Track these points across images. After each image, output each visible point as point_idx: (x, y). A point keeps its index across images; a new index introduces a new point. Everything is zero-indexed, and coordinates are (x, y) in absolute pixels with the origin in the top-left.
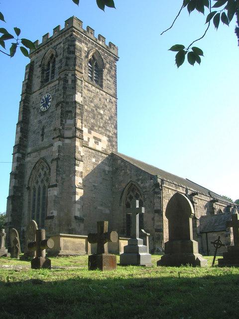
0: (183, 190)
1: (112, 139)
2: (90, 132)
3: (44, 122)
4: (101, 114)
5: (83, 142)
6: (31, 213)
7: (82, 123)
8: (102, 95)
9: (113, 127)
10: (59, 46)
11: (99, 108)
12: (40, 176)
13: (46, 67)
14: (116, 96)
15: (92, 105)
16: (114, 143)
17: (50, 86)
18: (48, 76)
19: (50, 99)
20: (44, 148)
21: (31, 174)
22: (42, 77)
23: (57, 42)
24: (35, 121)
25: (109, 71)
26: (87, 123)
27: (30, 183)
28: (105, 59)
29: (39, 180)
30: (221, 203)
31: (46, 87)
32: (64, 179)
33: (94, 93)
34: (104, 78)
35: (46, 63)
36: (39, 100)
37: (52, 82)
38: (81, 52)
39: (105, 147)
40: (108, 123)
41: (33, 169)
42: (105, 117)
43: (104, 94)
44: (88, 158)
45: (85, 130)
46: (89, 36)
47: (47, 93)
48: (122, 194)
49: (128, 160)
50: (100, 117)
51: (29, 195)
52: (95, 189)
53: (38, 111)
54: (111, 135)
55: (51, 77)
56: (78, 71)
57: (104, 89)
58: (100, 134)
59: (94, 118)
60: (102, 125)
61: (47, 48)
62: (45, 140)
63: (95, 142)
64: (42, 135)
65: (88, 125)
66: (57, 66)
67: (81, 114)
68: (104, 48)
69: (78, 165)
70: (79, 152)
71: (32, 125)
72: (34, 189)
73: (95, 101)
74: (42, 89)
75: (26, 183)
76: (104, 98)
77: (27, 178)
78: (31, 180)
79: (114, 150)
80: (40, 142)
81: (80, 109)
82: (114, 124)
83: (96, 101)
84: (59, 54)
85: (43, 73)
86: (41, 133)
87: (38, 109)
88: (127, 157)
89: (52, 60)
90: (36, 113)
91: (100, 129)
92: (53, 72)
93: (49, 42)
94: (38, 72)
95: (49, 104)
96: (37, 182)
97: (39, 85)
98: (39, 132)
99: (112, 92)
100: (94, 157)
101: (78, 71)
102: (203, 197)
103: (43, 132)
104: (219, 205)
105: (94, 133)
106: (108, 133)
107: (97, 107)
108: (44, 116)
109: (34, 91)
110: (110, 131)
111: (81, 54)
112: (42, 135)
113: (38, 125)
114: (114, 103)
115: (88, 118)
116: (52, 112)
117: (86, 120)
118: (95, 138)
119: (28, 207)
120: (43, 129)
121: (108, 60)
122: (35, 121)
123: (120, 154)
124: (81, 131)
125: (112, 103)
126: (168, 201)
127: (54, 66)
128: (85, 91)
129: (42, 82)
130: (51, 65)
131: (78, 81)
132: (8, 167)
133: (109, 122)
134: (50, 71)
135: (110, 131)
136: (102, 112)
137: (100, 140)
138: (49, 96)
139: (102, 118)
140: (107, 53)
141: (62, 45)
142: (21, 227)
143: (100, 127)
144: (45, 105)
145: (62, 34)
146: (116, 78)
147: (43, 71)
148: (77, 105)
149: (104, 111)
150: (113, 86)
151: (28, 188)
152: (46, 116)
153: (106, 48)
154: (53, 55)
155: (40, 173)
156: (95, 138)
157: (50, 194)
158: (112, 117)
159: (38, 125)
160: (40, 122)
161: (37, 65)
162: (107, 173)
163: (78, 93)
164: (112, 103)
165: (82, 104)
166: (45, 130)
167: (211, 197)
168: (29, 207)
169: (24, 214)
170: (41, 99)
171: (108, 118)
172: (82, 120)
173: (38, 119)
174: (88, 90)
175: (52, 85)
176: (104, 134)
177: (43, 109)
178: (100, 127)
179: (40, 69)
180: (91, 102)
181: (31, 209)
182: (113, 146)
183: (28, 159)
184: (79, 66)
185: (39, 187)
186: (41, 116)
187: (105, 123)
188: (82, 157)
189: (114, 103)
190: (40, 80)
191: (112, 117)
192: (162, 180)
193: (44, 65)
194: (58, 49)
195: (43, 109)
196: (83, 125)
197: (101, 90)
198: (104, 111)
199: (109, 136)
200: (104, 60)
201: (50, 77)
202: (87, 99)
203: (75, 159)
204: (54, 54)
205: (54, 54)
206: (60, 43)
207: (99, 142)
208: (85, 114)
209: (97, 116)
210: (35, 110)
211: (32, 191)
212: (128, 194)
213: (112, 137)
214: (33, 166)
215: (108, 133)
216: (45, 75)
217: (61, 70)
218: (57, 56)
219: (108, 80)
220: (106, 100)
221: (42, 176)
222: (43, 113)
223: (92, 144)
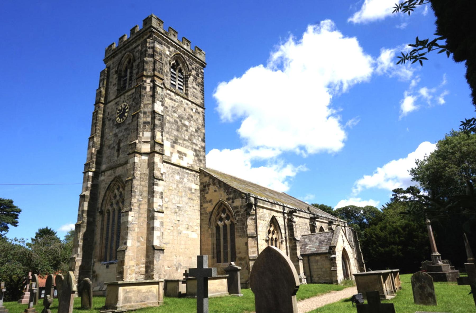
0: (280, 208)
1: (199, 153)
2: (173, 147)
3: (120, 135)
4: (185, 125)
5: (164, 157)
6: (104, 241)
7: (162, 135)
8: (187, 104)
9: (200, 139)
10: (137, 49)
11: (183, 118)
12: (115, 197)
13: (123, 74)
14: (204, 105)
15: (176, 115)
16: (201, 158)
17: (127, 94)
18: (125, 83)
19: (127, 108)
20: (121, 165)
21: (105, 195)
22: (118, 85)
23: (134, 46)
24: (111, 134)
25: (195, 79)
26: (169, 136)
27: (104, 205)
28: (191, 65)
29: (114, 201)
30: (321, 219)
31: (123, 96)
32: (140, 201)
33: (177, 102)
34: (190, 85)
35: (124, 69)
36: (115, 110)
37: (129, 90)
38: (162, 56)
39: (191, 162)
40: (194, 136)
41: (107, 189)
42: (191, 128)
43: (190, 103)
44: (170, 175)
45: (167, 145)
46: (171, 38)
47: (123, 102)
48: (211, 215)
49: (221, 179)
50: (184, 128)
51: (103, 221)
52: (179, 210)
53: (113, 123)
54: (197, 148)
55: (129, 84)
56: (158, 77)
57: (190, 99)
58: (186, 147)
59: (178, 130)
60: (187, 138)
61: (123, 52)
62: (120, 156)
63: (180, 157)
64: (118, 150)
65: (171, 138)
66: (135, 72)
67: (162, 126)
68: (189, 52)
69: (157, 185)
70: (159, 170)
71: (106, 139)
72: (109, 213)
73: (179, 111)
74: (119, 99)
75: (99, 206)
76: (189, 108)
77: (100, 201)
78: (104, 202)
79: (202, 165)
80: (116, 158)
81: (159, 120)
82: (202, 137)
83: (180, 111)
84: (136, 58)
85: (119, 80)
86: (116, 147)
87: (114, 120)
88: (217, 173)
89: (130, 66)
90: (111, 125)
91: (185, 142)
92: (131, 79)
93: (126, 44)
94: (114, 78)
95: (126, 114)
96: (112, 205)
97: (116, 94)
98: (114, 147)
99: (199, 101)
100: (178, 173)
101: (158, 77)
102: (302, 214)
103: (119, 146)
104: (320, 222)
105: (178, 148)
106: (194, 147)
107: (181, 118)
108: (120, 129)
109: (110, 100)
110: (196, 145)
111: (161, 58)
112: (118, 150)
113: (113, 139)
114: (201, 113)
115: (170, 130)
116: (129, 124)
117: (168, 133)
118: (179, 152)
119: (101, 234)
120: (119, 144)
121: (193, 66)
122: (111, 134)
123: (210, 170)
124: (162, 145)
125: (199, 113)
126: (86, 225)
127: (131, 73)
128: (167, 101)
129: (118, 90)
130: (129, 71)
131: (158, 88)
132: (254, 182)
133: (196, 134)
134: (128, 77)
135: (196, 145)
136: (187, 123)
137: (185, 155)
138: (126, 105)
139: (187, 131)
140: (193, 59)
141: (140, 47)
142: (91, 259)
143: (185, 140)
144: (121, 116)
145: (140, 34)
146: (203, 86)
147: (120, 78)
148: (157, 115)
149: (190, 122)
150: (200, 95)
151: (102, 212)
152: (124, 127)
153: (191, 52)
154: (130, 59)
155: (115, 194)
156: (179, 152)
157: (123, 219)
158: (199, 129)
159: (113, 139)
160: (116, 135)
161: (112, 71)
162: (193, 191)
163: (158, 102)
164: (199, 113)
165: (162, 114)
166: (122, 145)
167: (311, 213)
168: (102, 234)
169: (95, 243)
170: (117, 109)
171: (194, 130)
172: (162, 132)
173: (114, 132)
174: (171, 99)
175: (130, 93)
176: (190, 148)
177: (119, 120)
178: (185, 140)
179: (115, 76)
180: (174, 112)
181: (105, 236)
182: (200, 160)
183: (102, 178)
184: (159, 72)
185: (114, 209)
186: (117, 128)
187: (191, 135)
188: (162, 174)
189: (201, 113)
190: (116, 88)
191: (199, 129)
192: (256, 199)
193: (121, 71)
194: (136, 52)
195: (119, 120)
196: (165, 138)
197: (185, 99)
198: (190, 122)
199: (195, 151)
200: (189, 66)
201: (127, 85)
202: (170, 109)
203: (154, 177)
204: (132, 58)
205: (132, 58)
206: (138, 46)
207: (184, 157)
208: (167, 125)
209: (182, 128)
210: (111, 121)
211: (106, 214)
212: (217, 215)
213: (200, 151)
214: (107, 186)
215: (194, 147)
216: (122, 83)
217: (137, 76)
218: (134, 60)
219: (194, 88)
220: (192, 110)
221: (118, 198)
222: (118, 125)
223: (175, 159)
